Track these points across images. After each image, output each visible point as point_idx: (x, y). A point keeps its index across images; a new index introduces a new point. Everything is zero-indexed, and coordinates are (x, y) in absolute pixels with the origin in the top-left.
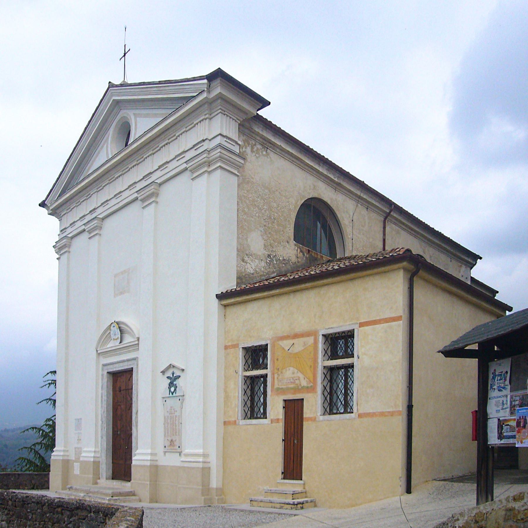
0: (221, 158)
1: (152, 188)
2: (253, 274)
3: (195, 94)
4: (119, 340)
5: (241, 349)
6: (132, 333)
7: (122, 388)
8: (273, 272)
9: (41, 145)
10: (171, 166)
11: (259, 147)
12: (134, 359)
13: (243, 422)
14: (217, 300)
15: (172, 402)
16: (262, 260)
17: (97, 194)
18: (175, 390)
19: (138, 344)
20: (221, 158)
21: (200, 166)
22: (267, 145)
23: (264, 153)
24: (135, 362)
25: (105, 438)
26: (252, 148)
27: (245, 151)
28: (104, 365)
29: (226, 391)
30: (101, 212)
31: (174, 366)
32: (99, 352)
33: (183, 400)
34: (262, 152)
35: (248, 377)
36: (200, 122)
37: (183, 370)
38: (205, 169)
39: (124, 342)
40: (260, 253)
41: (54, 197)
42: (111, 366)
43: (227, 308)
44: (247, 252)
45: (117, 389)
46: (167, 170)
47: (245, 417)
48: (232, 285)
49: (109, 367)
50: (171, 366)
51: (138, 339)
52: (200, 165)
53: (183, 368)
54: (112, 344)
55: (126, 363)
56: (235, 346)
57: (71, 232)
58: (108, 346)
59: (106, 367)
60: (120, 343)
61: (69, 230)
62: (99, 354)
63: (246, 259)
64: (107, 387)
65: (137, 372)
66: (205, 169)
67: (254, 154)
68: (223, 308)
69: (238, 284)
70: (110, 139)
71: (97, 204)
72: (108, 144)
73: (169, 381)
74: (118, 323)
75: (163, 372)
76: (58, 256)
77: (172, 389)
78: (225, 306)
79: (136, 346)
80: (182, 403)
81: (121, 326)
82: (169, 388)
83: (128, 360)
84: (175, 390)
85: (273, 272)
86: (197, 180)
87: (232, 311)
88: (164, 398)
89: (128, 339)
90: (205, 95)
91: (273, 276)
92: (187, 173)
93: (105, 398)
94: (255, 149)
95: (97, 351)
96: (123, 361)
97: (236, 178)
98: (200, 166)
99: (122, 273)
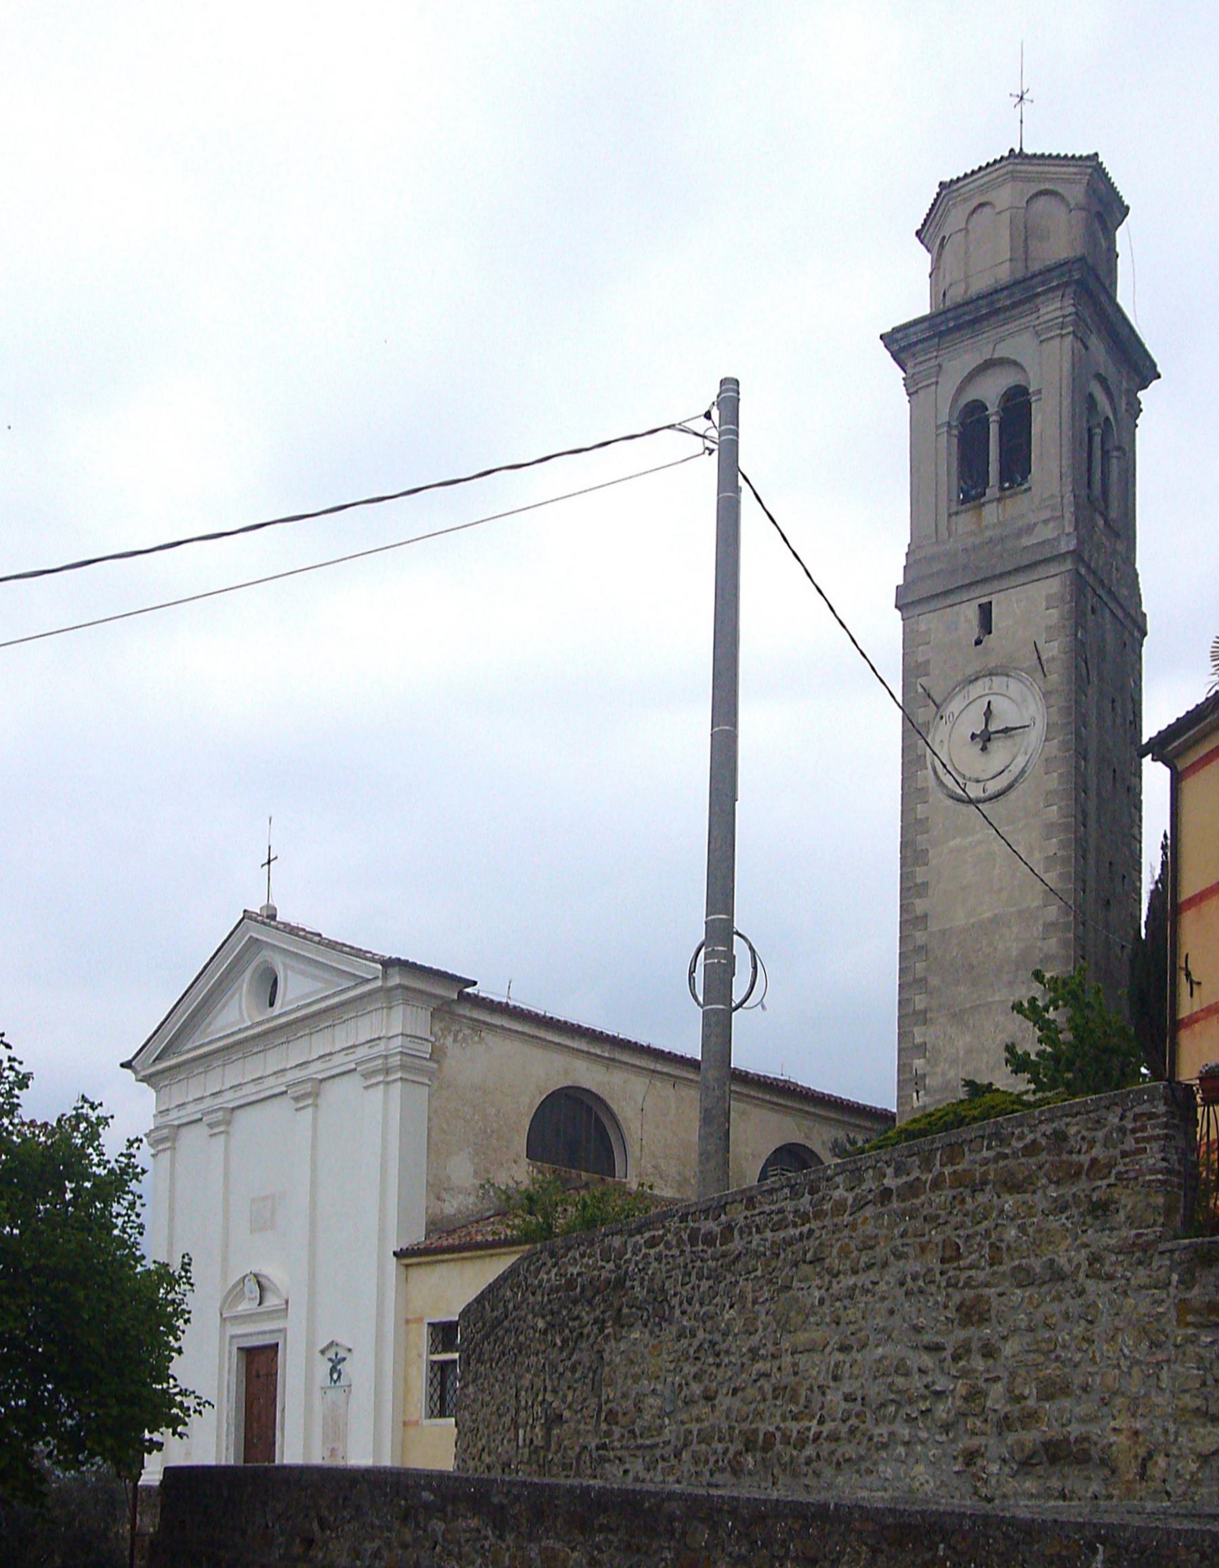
0: (403, 1067)
1: (308, 1087)
2: (455, 1215)
3: (370, 977)
4: (258, 1301)
5: (426, 1325)
6: (276, 1291)
7: (262, 1373)
8: (489, 1209)
9: (6, 428)
10: (338, 1059)
11: (467, 1032)
12: (280, 1331)
13: (427, 1422)
14: (395, 1259)
15: (333, 1395)
16: (469, 1194)
17: (224, 1071)
18: (339, 1377)
19: (287, 1309)
20: (403, 1067)
21: (374, 1073)
22: (478, 1026)
23: (476, 1039)
24: (282, 1335)
25: (232, 1449)
26: (456, 1036)
27: (444, 1044)
28: (232, 1337)
29: (406, 1380)
30: (230, 1099)
31: (337, 1345)
32: (224, 1316)
33: (350, 1392)
34: (472, 1039)
35: (435, 1362)
36: (376, 1010)
37: (350, 1350)
38: (381, 1078)
39: (266, 1304)
40: (467, 1185)
41: (148, 1058)
42: (245, 1339)
43: (410, 1269)
44: (446, 1186)
45: (254, 1372)
46: (328, 1065)
47: (431, 1415)
48: (417, 1236)
49: (241, 1340)
50: (332, 1344)
51: (287, 1302)
52: (373, 1072)
53: (350, 1347)
54: (244, 1307)
55: (267, 1336)
56: (421, 1320)
57: (175, 1117)
58: (240, 1308)
59: (235, 1340)
60: (260, 1304)
61: (174, 1114)
62: (224, 1320)
63: (444, 1195)
64: (237, 1371)
65: (285, 1349)
66: (381, 1078)
67: (459, 1044)
68: (403, 1269)
69: (427, 1236)
70: (245, 987)
71: (223, 1084)
72: (241, 995)
73: (331, 1365)
74: (256, 1276)
75: (323, 1352)
76: (152, 1151)
77: (335, 1376)
78: (407, 1266)
79: (284, 1311)
80: (348, 1397)
81: (260, 1279)
82: (331, 1375)
83: (272, 1332)
84: (339, 1377)
85: (489, 1209)
86: (370, 1090)
87: (414, 1272)
88: (322, 1388)
89: (272, 1301)
90: (379, 983)
91: (488, 1214)
92: (356, 1077)
93: (233, 1387)
94: (461, 1035)
95: (221, 1315)
96: (263, 1333)
97: (427, 1088)
98: (374, 1073)
99: (265, 1198)
